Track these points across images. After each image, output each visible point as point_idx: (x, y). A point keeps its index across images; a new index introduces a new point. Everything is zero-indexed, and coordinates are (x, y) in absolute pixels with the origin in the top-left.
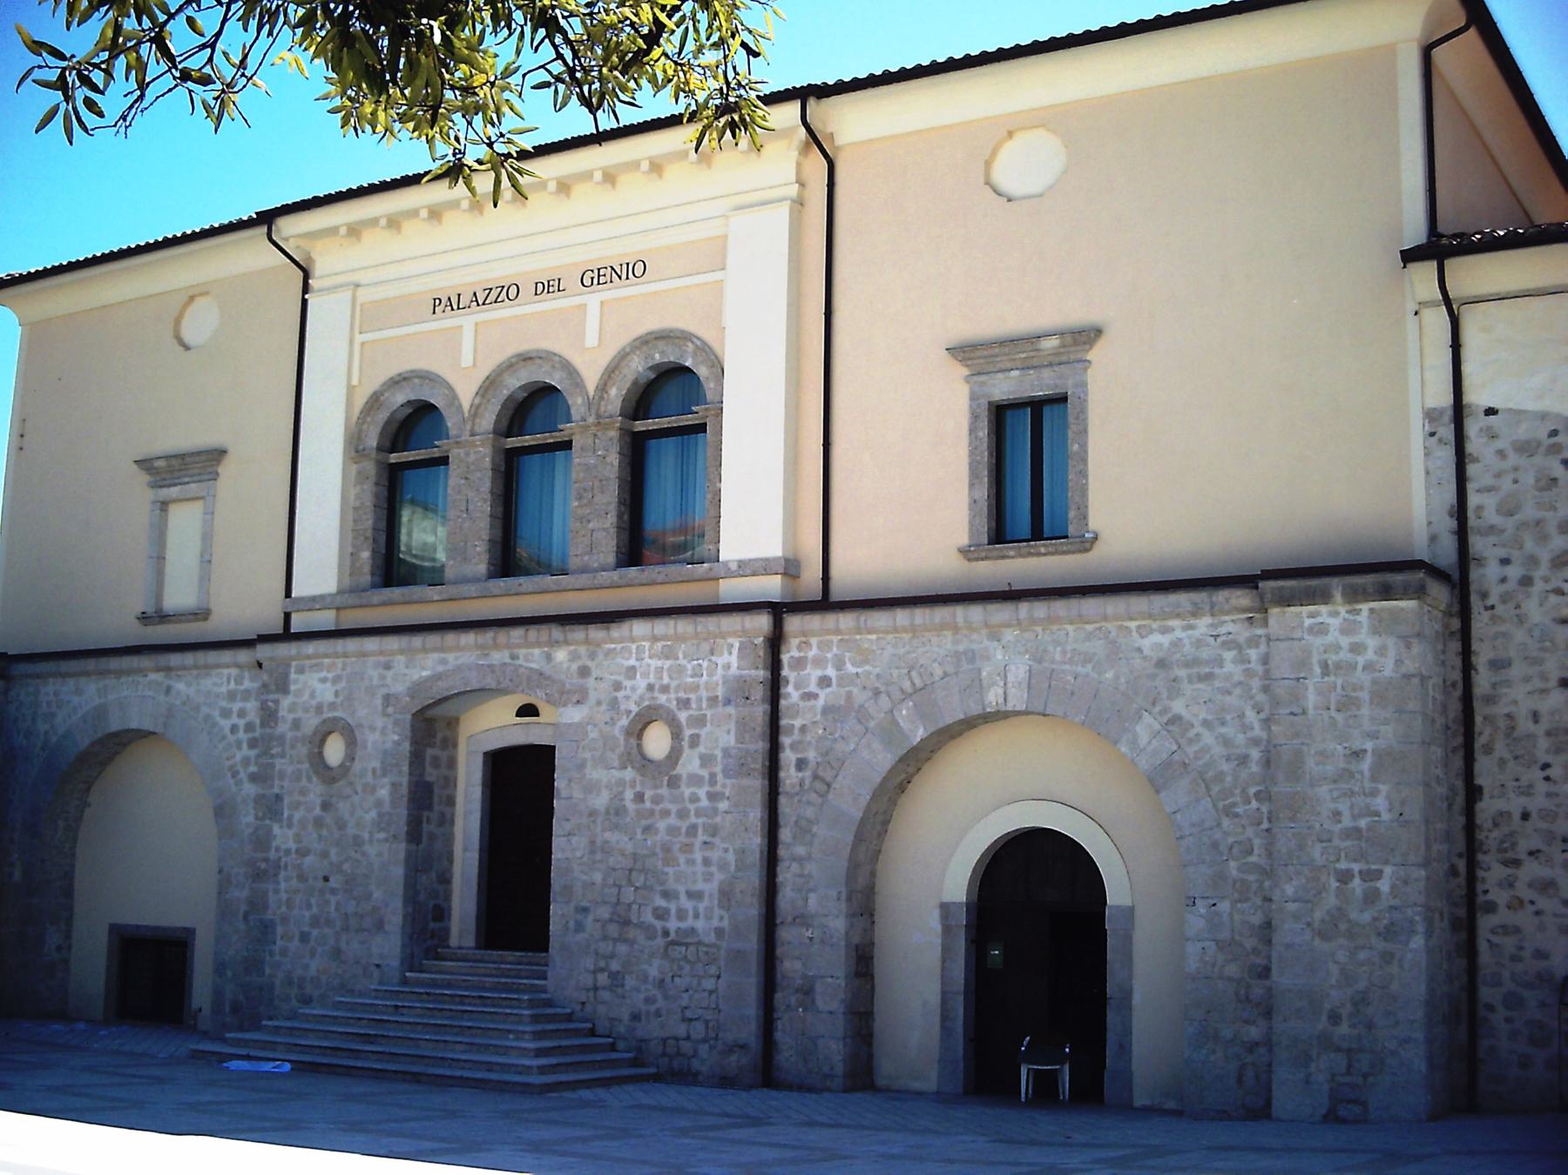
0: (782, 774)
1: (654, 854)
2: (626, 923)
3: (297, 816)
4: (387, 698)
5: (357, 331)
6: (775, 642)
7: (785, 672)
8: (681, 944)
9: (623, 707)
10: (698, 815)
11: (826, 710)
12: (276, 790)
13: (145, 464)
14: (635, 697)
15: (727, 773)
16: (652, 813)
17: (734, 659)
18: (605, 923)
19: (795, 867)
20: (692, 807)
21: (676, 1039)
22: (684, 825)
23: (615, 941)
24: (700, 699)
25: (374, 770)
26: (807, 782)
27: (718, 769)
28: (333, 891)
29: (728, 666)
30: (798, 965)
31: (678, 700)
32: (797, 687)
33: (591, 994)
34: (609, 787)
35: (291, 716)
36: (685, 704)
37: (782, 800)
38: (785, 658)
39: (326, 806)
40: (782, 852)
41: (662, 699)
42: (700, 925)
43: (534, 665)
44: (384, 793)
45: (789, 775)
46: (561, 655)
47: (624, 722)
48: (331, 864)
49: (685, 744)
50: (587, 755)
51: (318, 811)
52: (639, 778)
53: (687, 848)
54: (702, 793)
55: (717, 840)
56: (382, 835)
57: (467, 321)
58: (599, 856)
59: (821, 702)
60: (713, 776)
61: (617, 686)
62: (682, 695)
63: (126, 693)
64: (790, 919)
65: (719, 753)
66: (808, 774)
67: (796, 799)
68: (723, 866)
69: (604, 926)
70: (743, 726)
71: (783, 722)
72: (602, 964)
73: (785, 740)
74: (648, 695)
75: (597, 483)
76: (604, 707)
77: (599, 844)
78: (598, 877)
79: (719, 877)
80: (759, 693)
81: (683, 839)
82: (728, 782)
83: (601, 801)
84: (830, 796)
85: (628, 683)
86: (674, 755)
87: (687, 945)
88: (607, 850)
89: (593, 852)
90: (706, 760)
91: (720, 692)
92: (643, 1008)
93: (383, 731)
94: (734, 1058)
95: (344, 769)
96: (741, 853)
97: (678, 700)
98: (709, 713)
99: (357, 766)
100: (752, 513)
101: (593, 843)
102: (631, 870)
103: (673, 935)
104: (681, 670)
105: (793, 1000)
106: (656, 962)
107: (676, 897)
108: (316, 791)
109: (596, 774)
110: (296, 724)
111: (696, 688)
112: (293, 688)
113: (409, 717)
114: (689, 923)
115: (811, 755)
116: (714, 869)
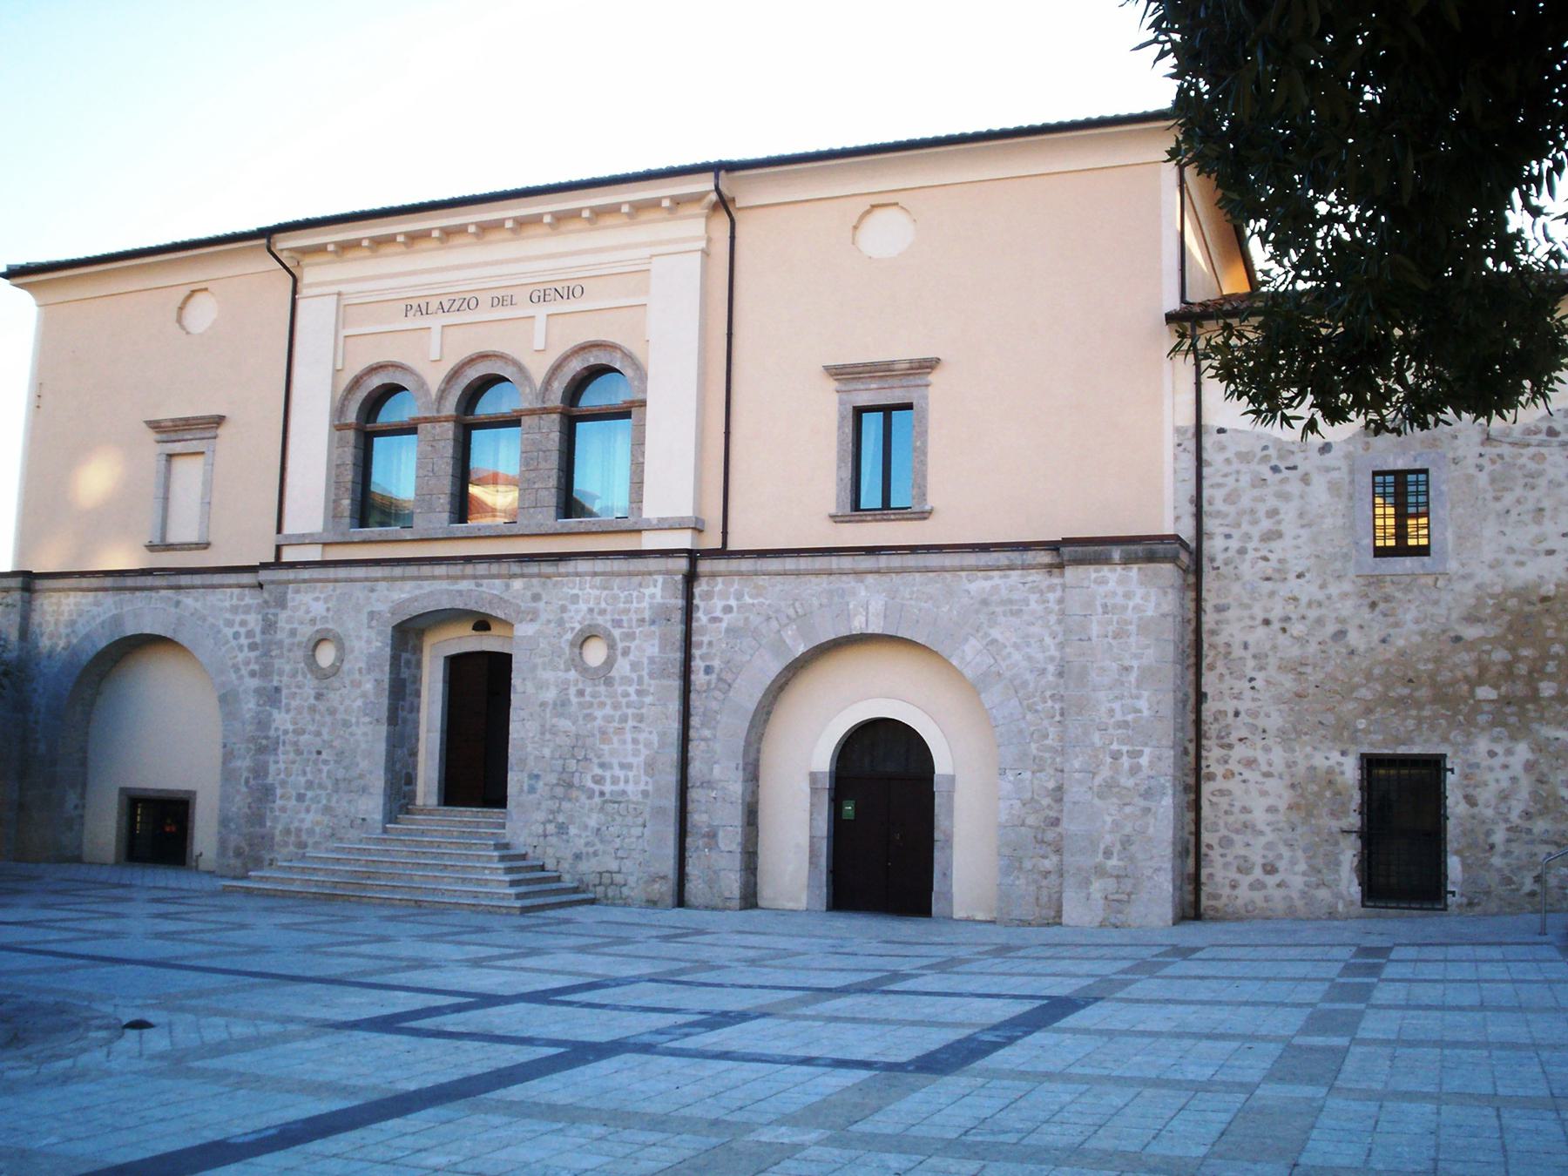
0: (693, 677)
2: (570, 785)
3: (294, 704)
4: (372, 615)
6: (691, 578)
7: (696, 601)
9: (568, 625)
10: (628, 706)
11: (728, 630)
12: (275, 683)
13: (155, 426)
16: (591, 705)
17: (658, 591)
20: (624, 701)
24: (630, 620)
25: (360, 670)
27: (645, 673)
28: (326, 762)
35: (288, 627)
36: (618, 623)
37: (693, 696)
38: (697, 591)
39: (319, 696)
40: (692, 734)
41: (600, 620)
42: (630, 788)
44: (368, 686)
45: (699, 678)
46: (517, 584)
47: (569, 636)
49: (619, 652)
50: (539, 661)
51: (312, 701)
53: (620, 731)
54: (631, 690)
56: (367, 719)
57: (436, 322)
58: (548, 736)
59: (724, 625)
61: (564, 609)
65: (646, 661)
66: (714, 677)
68: (648, 745)
73: (696, 652)
78: (547, 752)
79: (644, 752)
80: (678, 616)
83: (550, 695)
84: (731, 694)
86: (609, 662)
88: (554, 731)
89: (543, 733)
90: (635, 666)
91: (647, 615)
93: (369, 642)
94: (657, 886)
95: (335, 670)
96: (662, 735)
99: (346, 666)
101: (543, 726)
103: (608, 796)
105: (701, 843)
106: (595, 816)
108: (310, 685)
110: (293, 633)
112: (290, 604)
114: (621, 786)
115: (716, 663)
116: (641, 746)
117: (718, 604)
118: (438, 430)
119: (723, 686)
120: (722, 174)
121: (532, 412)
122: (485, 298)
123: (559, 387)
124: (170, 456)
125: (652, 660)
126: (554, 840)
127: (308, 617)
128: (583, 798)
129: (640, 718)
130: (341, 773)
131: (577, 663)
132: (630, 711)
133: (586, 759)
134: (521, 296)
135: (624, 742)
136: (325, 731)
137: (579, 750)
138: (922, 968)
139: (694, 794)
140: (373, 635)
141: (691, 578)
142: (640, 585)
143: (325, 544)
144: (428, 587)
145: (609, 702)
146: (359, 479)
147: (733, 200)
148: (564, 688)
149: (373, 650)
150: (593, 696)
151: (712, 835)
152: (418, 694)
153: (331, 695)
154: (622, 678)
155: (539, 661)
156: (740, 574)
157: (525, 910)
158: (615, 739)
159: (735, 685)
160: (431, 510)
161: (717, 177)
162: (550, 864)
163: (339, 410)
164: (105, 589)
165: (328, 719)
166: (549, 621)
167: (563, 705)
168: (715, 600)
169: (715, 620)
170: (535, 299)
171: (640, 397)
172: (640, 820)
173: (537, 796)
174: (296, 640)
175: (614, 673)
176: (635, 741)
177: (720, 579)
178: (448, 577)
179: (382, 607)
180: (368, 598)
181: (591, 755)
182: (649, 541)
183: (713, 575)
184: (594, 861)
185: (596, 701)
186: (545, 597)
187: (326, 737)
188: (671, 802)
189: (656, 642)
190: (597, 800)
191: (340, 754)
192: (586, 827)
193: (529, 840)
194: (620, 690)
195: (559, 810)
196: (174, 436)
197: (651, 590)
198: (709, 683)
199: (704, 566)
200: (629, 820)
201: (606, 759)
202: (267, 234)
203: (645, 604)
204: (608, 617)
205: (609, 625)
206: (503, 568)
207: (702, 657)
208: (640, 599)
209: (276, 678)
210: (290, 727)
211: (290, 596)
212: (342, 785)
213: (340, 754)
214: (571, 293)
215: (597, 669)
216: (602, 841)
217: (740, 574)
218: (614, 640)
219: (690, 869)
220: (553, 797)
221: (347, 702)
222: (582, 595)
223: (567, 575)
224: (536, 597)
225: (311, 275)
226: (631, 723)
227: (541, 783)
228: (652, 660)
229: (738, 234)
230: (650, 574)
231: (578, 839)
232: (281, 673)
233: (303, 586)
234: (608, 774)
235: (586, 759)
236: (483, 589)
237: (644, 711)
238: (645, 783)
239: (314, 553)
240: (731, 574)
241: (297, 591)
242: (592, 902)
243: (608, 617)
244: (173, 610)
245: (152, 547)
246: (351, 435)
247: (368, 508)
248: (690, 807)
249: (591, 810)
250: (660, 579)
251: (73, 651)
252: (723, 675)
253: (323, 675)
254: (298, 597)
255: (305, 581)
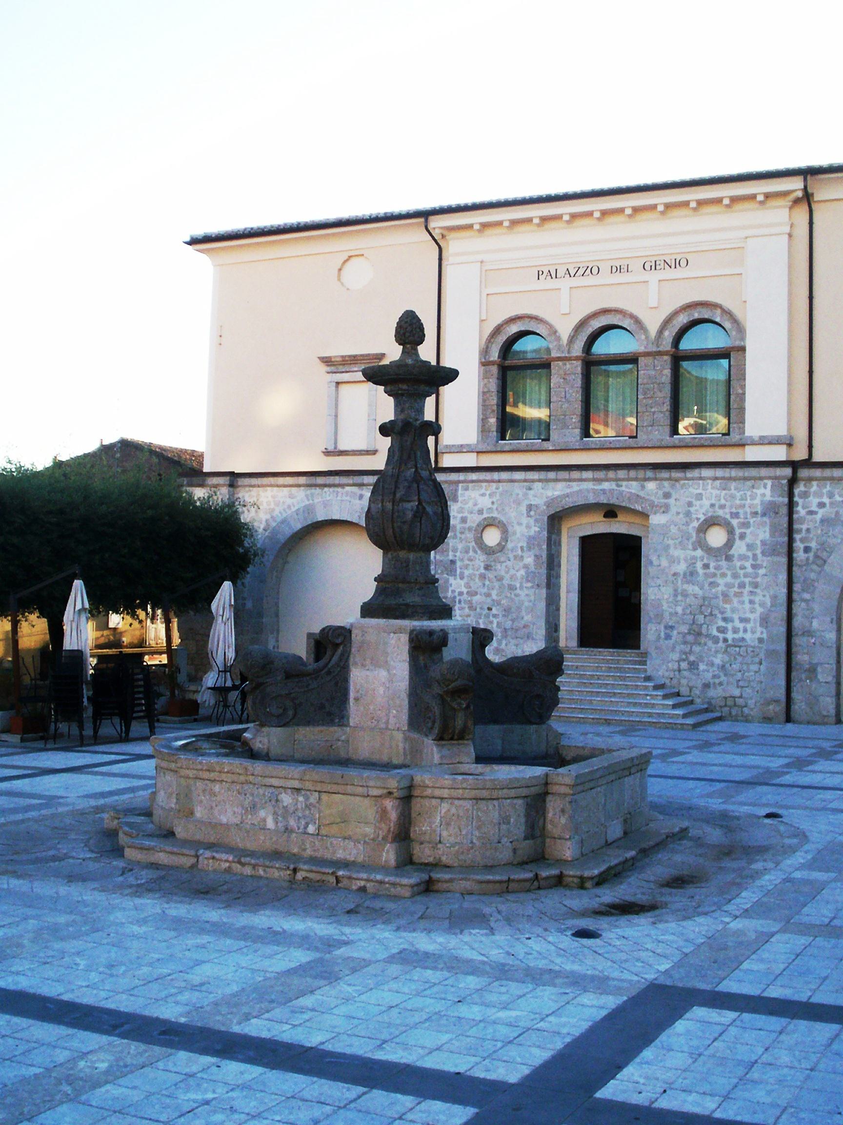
0: (795, 555)
1: (717, 597)
2: (699, 634)
3: (467, 573)
4: (530, 507)
5: (483, 286)
6: (793, 482)
7: (796, 499)
8: (736, 646)
9: (694, 516)
10: (745, 576)
11: (822, 521)
12: (451, 557)
13: (327, 361)
14: (703, 511)
15: (763, 553)
16: (714, 575)
17: (768, 492)
18: (684, 635)
19: (803, 605)
20: (742, 572)
21: (734, 697)
22: (737, 582)
23: (692, 644)
24: (746, 513)
25: (522, 548)
26: (811, 559)
27: (758, 552)
28: (495, 616)
29: (764, 495)
30: (806, 657)
31: (731, 513)
32: (803, 508)
33: (677, 673)
34: (686, 560)
35: (460, 515)
36: (735, 515)
37: (795, 568)
38: (796, 491)
39: (487, 567)
40: (795, 596)
41: (720, 513)
42: (748, 636)
43: (633, 491)
44: (529, 560)
45: (800, 555)
46: (651, 486)
47: (696, 524)
48: (493, 600)
49: (737, 537)
50: (671, 542)
51: (482, 571)
52: (706, 556)
53: (739, 595)
54: (748, 564)
55: (758, 591)
56: (530, 585)
57: (564, 284)
58: (679, 598)
59: (818, 517)
60: (755, 556)
61: (690, 504)
62: (734, 510)
63: (328, 498)
64: (800, 633)
65: (758, 543)
66: (811, 555)
67: (804, 568)
68: (762, 604)
69: (684, 637)
70: (774, 530)
71: (795, 526)
72: (684, 657)
73: (797, 537)
74: (711, 510)
75: (656, 386)
76: (681, 516)
77: (679, 591)
78: (679, 610)
79: (759, 610)
80: (784, 510)
81: (736, 589)
82: (765, 558)
83: (681, 568)
84: (826, 567)
85: (698, 503)
86: (729, 544)
87: (740, 647)
88: (685, 595)
89: (676, 595)
90: (750, 547)
91: (759, 509)
92: (711, 681)
93: (528, 527)
94: (771, 707)
95: (501, 547)
96: (774, 597)
97: (731, 513)
98: (752, 521)
99: (510, 545)
100: (768, 410)
101: (676, 590)
102: (701, 606)
103: (730, 642)
104: (733, 497)
105: (803, 676)
106: (720, 656)
107: (732, 621)
108: (480, 559)
109: (677, 553)
110: (464, 520)
111: (744, 506)
112: (460, 499)
113: (546, 518)
114: (741, 635)
115: (813, 545)
116: (757, 606)
117: (814, 501)
118: (568, 366)
119: (820, 562)
120: (809, 177)
121: (647, 354)
122: (605, 268)
123: (668, 336)
124: (338, 383)
125: (763, 543)
126: (685, 673)
127: (476, 508)
128: (710, 643)
129: (756, 585)
130: (508, 624)
131: (701, 544)
132: (747, 580)
133: (711, 614)
134: (636, 266)
135: (743, 603)
136: (494, 593)
137: (706, 607)
138: (688, 748)
139: (797, 640)
140: (532, 521)
141: (793, 482)
142: (753, 487)
143: (478, 452)
144: (575, 487)
145: (729, 573)
146: (500, 403)
147: (813, 194)
148: (692, 562)
149: (532, 533)
150: (716, 568)
151: (812, 671)
152: (560, 566)
153: (498, 566)
154: (740, 555)
155: (671, 542)
156: (832, 479)
157: (695, 726)
158: (735, 600)
159: (829, 561)
160: (565, 426)
161: (805, 180)
162: (684, 690)
163: (485, 351)
164: (299, 486)
165: (497, 584)
166: (678, 513)
167: (692, 574)
168: (811, 498)
169: (811, 513)
170: (647, 267)
171: (738, 343)
172: (757, 660)
173: (672, 642)
174: (467, 525)
175: (732, 552)
176: (751, 602)
177: (814, 483)
178: (594, 480)
179: (540, 501)
180: (525, 495)
181: (716, 612)
182: (752, 454)
183: (810, 479)
184: (720, 689)
185: (718, 573)
186: (674, 496)
187: (494, 597)
188: (782, 647)
189: (767, 529)
190: (721, 644)
191: (507, 611)
192: (712, 665)
193: (667, 674)
194: (738, 564)
195: (691, 652)
196: (341, 368)
197: (761, 491)
198: (808, 559)
199: (803, 473)
200: (749, 659)
201: (728, 614)
202: (425, 215)
203: (757, 501)
204: (727, 510)
205: (728, 517)
206: (641, 474)
207: (802, 540)
208: (753, 497)
209: (451, 553)
210: (465, 590)
211: (460, 492)
212: (509, 633)
213: (507, 611)
214: (677, 263)
215: (719, 549)
216: (725, 675)
217: (832, 479)
218: (733, 528)
219: (794, 695)
220: (685, 643)
221: (512, 572)
222: (705, 495)
223: (692, 479)
224: (667, 495)
225: (454, 246)
226: (748, 588)
227: (675, 632)
228: (763, 543)
229: (815, 220)
230: (761, 479)
231: (706, 672)
232: (455, 550)
233: (470, 485)
234: (730, 626)
235: (711, 614)
236: (623, 488)
237: (759, 580)
238: (760, 632)
239: (470, 460)
240: (825, 479)
241: (467, 489)
242: (720, 719)
243: (727, 510)
244: (358, 502)
245: (327, 453)
246: (494, 369)
247: (507, 425)
248: (794, 650)
249: (717, 652)
250: (769, 483)
251: (274, 533)
252: (819, 553)
253: (489, 551)
254: (467, 493)
255: (473, 481)
